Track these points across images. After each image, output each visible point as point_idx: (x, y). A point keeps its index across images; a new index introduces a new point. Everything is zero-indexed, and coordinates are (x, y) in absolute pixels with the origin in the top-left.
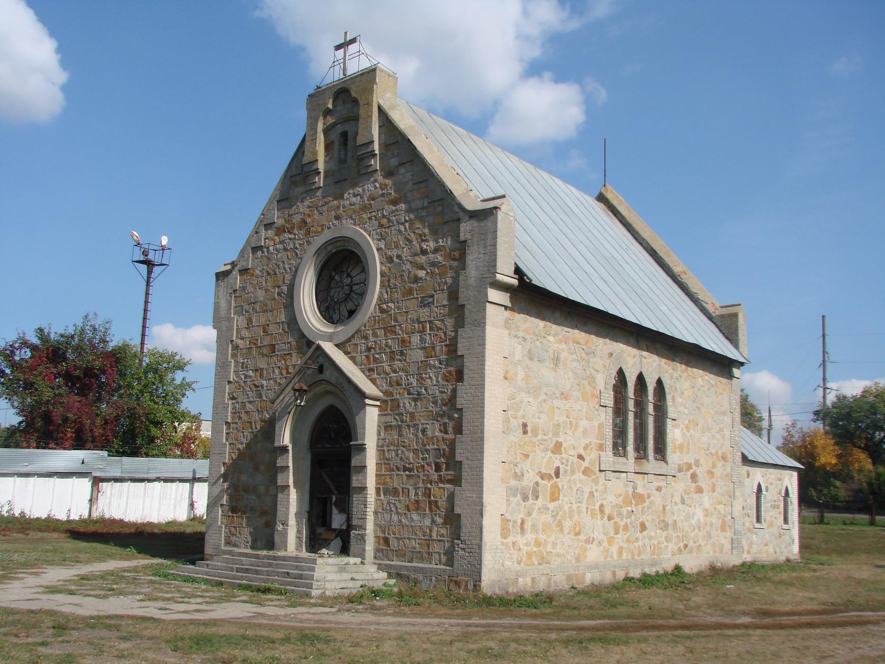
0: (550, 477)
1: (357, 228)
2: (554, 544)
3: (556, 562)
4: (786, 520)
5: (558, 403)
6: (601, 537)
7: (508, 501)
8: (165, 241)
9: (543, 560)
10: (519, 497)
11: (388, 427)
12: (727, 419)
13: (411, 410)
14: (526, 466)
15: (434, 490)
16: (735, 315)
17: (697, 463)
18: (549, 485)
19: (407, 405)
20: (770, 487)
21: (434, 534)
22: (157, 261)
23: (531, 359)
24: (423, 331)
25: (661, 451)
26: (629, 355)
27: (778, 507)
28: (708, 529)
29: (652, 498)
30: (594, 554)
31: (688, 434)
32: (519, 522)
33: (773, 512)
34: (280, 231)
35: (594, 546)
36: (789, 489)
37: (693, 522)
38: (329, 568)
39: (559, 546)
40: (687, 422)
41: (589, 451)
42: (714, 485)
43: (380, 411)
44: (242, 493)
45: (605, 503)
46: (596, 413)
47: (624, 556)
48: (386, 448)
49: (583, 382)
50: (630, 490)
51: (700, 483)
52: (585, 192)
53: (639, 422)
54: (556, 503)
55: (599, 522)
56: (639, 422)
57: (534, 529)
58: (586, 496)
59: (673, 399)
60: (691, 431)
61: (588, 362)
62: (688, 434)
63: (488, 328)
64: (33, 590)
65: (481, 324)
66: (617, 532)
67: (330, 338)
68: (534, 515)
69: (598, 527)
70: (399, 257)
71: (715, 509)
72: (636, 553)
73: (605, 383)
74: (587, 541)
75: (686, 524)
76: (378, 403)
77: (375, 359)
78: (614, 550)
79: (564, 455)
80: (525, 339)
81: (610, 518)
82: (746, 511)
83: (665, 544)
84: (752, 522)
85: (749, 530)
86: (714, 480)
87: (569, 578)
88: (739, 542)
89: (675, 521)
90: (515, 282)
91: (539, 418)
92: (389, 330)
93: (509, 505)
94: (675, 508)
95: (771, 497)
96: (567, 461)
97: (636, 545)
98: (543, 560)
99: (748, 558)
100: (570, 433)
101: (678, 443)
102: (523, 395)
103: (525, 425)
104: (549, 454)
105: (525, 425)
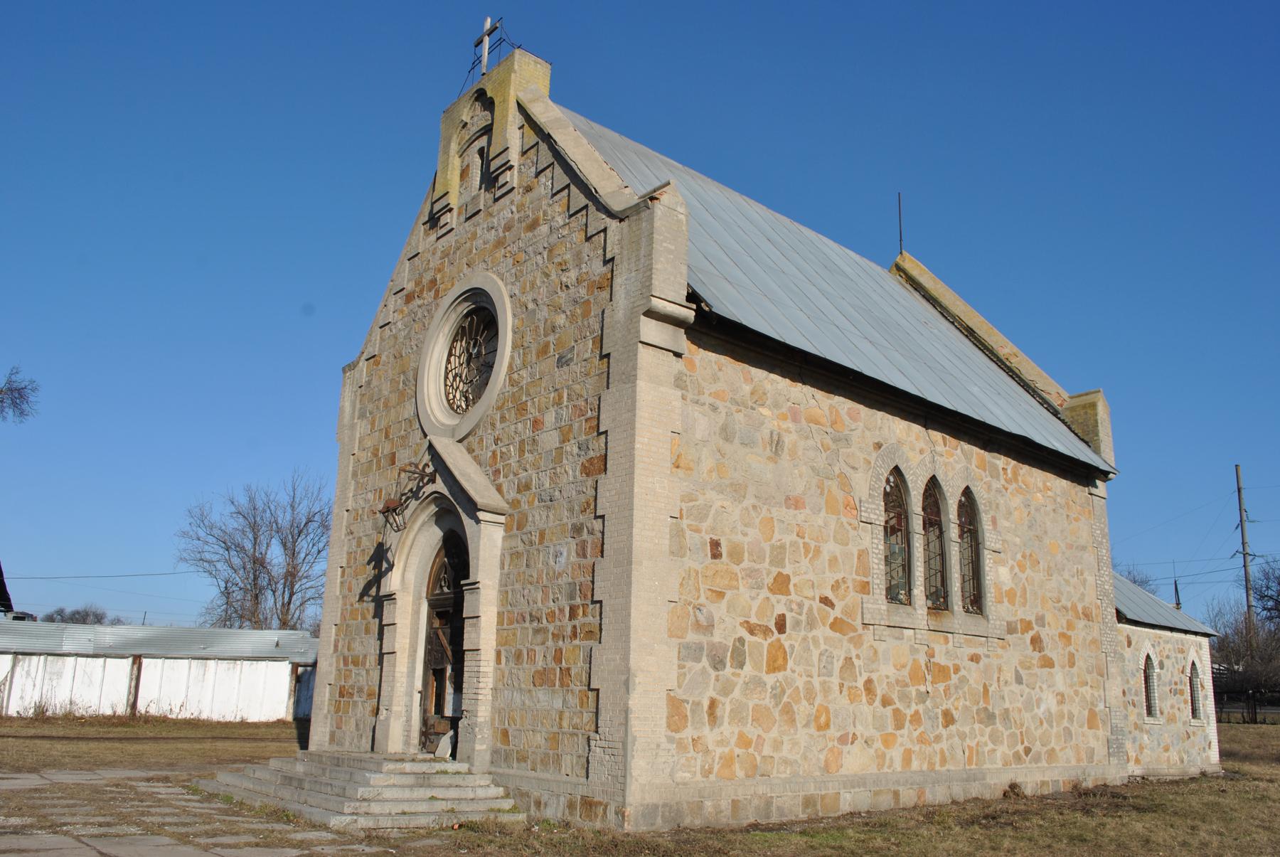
0: (766, 631)
2: (777, 745)
5: (779, 512)
6: (872, 732)
9: (753, 770)
10: (705, 662)
11: (515, 555)
12: (1089, 557)
13: (541, 526)
14: (719, 610)
16: (1093, 406)
18: (766, 644)
19: (537, 517)
20: (1166, 662)
21: (565, 724)
23: (727, 439)
24: (558, 403)
25: (976, 602)
26: (913, 449)
27: (1182, 692)
28: (1065, 723)
29: (963, 672)
30: (855, 761)
31: (1023, 576)
32: (706, 703)
33: (1172, 700)
35: (856, 748)
37: (1040, 712)
39: (786, 747)
40: (1019, 556)
41: (841, 591)
42: (1072, 656)
43: (506, 531)
45: (874, 677)
46: (852, 533)
47: (915, 765)
49: (827, 483)
50: (922, 659)
51: (1047, 652)
53: (932, 552)
54: (780, 675)
55: (865, 708)
57: (737, 714)
58: (838, 665)
60: (1028, 571)
62: (1023, 576)
65: (631, 378)
66: (899, 726)
68: (737, 693)
69: (866, 717)
70: (535, 301)
71: (1076, 693)
72: (937, 759)
74: (843, 740)
75: (1027, 715)
76: (502, 519)
78: (896, 754)
79: (793, 597)
80: (714, 408)
81: (886, 702)
82: (1129, 698)
83: (991, 746)
84: (1139, 715)
85: (1136, 726)
86: (1071, 649)
87: (808, 802)
89: (1007, 710)
91: (745, 535)
93: (681, 676)
94: (1006, 690)
96: (800, 605)
97: (937, 747)
98: (753, 770)
99: (1136, 770)
100: (805, 562)
101: (1005, 588)
102: (711, 495)
103: (715, 545)
104: (765, 593)
105: (715, 545)
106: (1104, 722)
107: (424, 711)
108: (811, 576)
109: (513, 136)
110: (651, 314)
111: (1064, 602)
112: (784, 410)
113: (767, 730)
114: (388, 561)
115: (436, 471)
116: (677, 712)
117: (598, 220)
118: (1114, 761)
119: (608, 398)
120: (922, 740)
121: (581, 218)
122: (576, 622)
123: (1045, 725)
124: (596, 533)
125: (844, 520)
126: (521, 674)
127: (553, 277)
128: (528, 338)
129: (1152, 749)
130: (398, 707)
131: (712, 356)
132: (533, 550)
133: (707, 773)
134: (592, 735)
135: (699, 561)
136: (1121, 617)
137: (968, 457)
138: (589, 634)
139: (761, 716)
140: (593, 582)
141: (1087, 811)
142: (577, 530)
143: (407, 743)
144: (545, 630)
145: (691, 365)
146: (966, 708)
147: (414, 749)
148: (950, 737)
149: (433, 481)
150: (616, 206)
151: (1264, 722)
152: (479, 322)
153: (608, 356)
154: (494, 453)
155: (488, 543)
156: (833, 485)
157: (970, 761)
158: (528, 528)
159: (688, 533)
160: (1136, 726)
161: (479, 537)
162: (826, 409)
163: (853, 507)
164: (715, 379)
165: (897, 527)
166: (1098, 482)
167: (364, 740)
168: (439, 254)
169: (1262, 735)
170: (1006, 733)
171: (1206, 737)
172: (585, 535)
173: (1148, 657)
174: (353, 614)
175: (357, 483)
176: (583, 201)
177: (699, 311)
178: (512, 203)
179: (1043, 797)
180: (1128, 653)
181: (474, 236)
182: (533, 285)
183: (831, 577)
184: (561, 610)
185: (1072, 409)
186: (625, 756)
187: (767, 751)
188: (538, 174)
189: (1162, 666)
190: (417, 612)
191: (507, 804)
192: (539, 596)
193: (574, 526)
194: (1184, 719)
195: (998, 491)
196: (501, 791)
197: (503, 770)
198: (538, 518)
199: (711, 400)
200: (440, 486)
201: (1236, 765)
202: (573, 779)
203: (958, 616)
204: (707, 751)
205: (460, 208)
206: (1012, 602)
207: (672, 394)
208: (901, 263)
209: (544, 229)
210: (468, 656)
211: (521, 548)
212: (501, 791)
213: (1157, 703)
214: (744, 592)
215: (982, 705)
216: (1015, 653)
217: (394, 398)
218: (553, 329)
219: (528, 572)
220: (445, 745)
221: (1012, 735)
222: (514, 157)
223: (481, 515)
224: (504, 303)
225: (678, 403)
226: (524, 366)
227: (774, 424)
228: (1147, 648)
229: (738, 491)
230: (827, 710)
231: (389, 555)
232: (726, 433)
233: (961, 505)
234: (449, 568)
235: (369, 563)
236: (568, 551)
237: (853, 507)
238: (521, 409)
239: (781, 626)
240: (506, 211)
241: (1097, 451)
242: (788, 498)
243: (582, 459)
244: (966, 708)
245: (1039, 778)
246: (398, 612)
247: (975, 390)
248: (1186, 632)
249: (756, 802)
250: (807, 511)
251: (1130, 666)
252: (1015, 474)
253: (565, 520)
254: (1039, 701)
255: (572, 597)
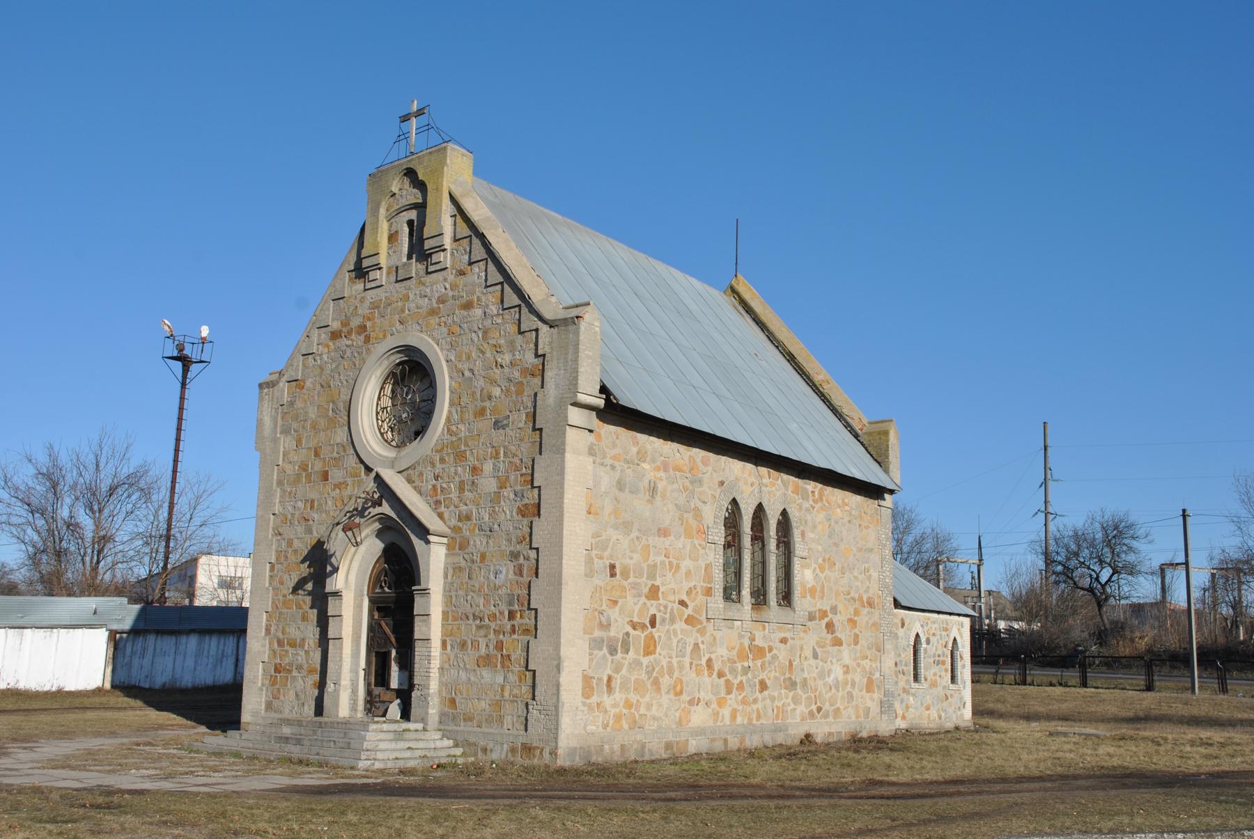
0: (643, 626)
1: (424, 336)
2: (649, 706)
3: (651, 726)
4: (953, 679)
5: (654, 540)
6: (710, 697)
7: (591, 654)
8: (205, 331)
9: (634, 725)
10: (605, 650)
11: (458, 569)
12: (875, 557)
13: (482, 549)
14: (614, 614)
15: (506, 639)
16: (886, 433)
17: (834, 610)
18: (643, 636)
19: (478, 543)
20: (932, 639)
21: (506, 694)
22: (195, 357)
23: (621, 489)
24: (497, 456)
25: (786, 597)
26: (746, 483)
27: (943, 663)
28: (849, 688)
29: (775, 651)
30: (699, 717)
31: (822, 576)
32: (605, 679)
33: (935, 669)
34: (335, 335)
35: (699, 708)
36: (959, 640)
37: (830, 680)
38: (382, 736)
39: (654, 708)
40: (820, 561)
41: (693, 595)
42: (856, 636)
43: (448, 549)
44: (287, 648)
45: (713, 656)
46: (702, 551)
47: (739, 720)
48: (453, 594)
49: (686, 515)
50: (746, 642)
51: (838, 634)
52: (710, 285)
53: (758, 560)
54: (651, 658)
55: (707, 680)
56: (758, 560)
57: (624, 686)
58: (689, 649)
59: (803, 534)
60: (827, 572)
61: (693, 492)
62: (822, 576)
63: (568, 456)
64: (30, 765)
65: (560, 450)
66: (729, 692)
67: (392, 464)
68: (624, 671)
69: (706, 686)
70: (471, 370)
71: (858, 665)
72: (754, 716)
73: (713, 516)
74: (691, 702)
75: (820, 683)
76: (445, 540)
77: (442, 489)
78: (726, 712)
79: (661, 601)
80: (613, 467)
81: (721, 675)
82: (900, 668)
83: (792, 706)
84: (907, 681)
85: (904, 690)
86: (856, 631)
87: (668, 746)
88: (891, 706)
89: (805, 679)
90: (601, 403)
91: (631, 558)
92: (460, 456)
93: (591, 660)
94: (805, 663)
95: (933, 650)
96: (666, 607)
97: (755, 707)
98: (634, 725)
99: (902, 724)
100: (669, 575)
101: (809, 586)
102: (611, 531)
103: (612, 567)
104: (643, 599)
105: (612, 567)
106: (879, 688)
107: (368, 685)
108: (673, 586)
109: (444, 223)
110: (576, 404)
111: (853, 594)
112: (658, 463)
113: (642, 697)
114: (332, 565)
115: (381, 497)
116: (588, 685)
117: (529, 322)
118: (885, 717)
119: (541, 463)
120: (744, 702)
121: (465, 242)
122: (515, 622)
123: (833, 690)
124: (532, 561)
125: (696, 542)
126: (466, 658)
127: (488, 355)
128: (464, 400)
129: (916, 708)
130: (345, 681)
131: (612, 428)
132: (475, 567)
133: (605, 726)
134: (530, 702)
135: (602, 579)
136: (897, 604)
137: (785, 484)
138: (526, 631)
139: (639, 687)
140: (529, 595)
141: (856, 751)
142: (514, 556)
143: (354, 708)
144: (488, 627)
145: (599, 437)
146: (776, 678)
147: (360, 714)
148: (764, 699)
149: (380, 505)
150: (548, 315)
151: (1032, 684)
152: (412, 372)
153: (541, 430)
154: (434, 486)
155: (435, 560)
156: (689, 517)
157: (777, 716)
158: (470, 549)
159: (596, 560)
160: (904, 690)
161: (429, 555)
162: (687, 459)
163: (703, 532)
164: (614, 445)
165: (732, 542)
166: (886, 496)
167: (306, 708)
168: (367, 304)
169: (1024, 696)
170: (804, 696)
171: (961, 698)
172: (521, 560)
173: (917, 635)
174: (286, 604)
175: (284, 491)
176: (517, 301)
177: (608, 400)
178: (445, 280)
179: (829, 744)
180: (901, 632)
181: (407, 298)
182: (469, 357)
183: (686, 585)
184: (501, 613)
185: (870, 434)
186: (557, 715)
187: (643, 711)
188: (470, 264)
189: (928, 642)
190: (359, 607)
191: (459, 751)
192: (482, 601)
193: (512, 553)
194: (944, 683)
195: (807, 510)
196: (451, 743)
197: (452, 727)
198: (478, 543)
199: (611, 462)
200: (386, 509)
201: (985, 721)
202: (515, 732)
203: (774, 608)
204: (606, 711)
205: (389, 268)
206: (813, 596)
207: (589, 461)
208: (736, 286)
209: (478, 312)
210: (418, 645)
211: (463, 564)
212: (451, 743)
213: (922, 671)
214: (630, 600)
215: (787, 675)
216: (814, 636)
217: (322, 423)
218: (490, 398)
219: (471, 583)
220: (394, 709)
221: (809, 698)
222: (447, 241)
223: (431, 538)
224: (441, 366)
225: (590, 467)
226: (462, 420)
227: (650, 475)
228: (917, 628)
229: (627, 527)
230: (681, 681)
231: (333, 560)
232: (620, 486)
233: (779, 523)
234: (389, 573)
235: (303, 562)
236: (507, 571)
237: (703, 532)
238: (460, 456)
239: (653, 623)
240: (438, 285)
241: (886, 471)
242: (659, 529)
243: (518, 504)
244: (776, 678)
245: (827, 730)
246: (344, 606)
247: (793, 426)
248: (950, 614)
249: (635, 746)
250: (672, 538)
251: (903, 643)
252: (821, 495)
253: (503, 547)
254: (830, 671)
255: (511, 603)
